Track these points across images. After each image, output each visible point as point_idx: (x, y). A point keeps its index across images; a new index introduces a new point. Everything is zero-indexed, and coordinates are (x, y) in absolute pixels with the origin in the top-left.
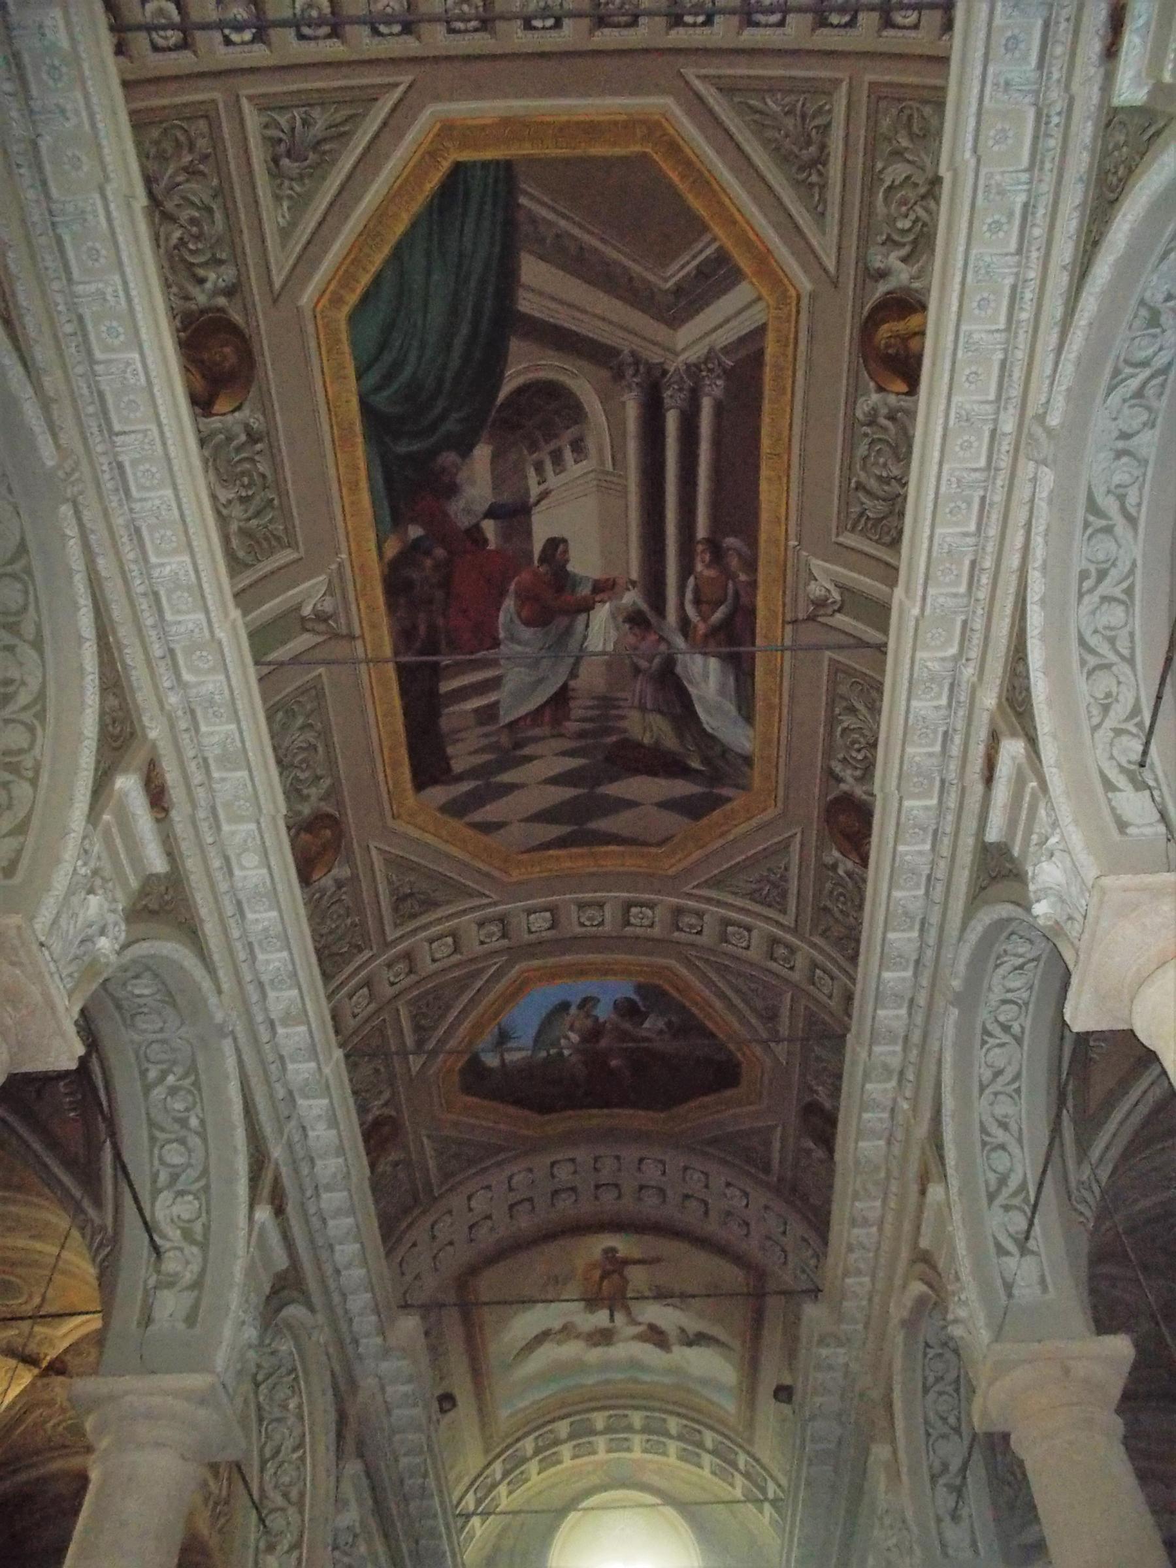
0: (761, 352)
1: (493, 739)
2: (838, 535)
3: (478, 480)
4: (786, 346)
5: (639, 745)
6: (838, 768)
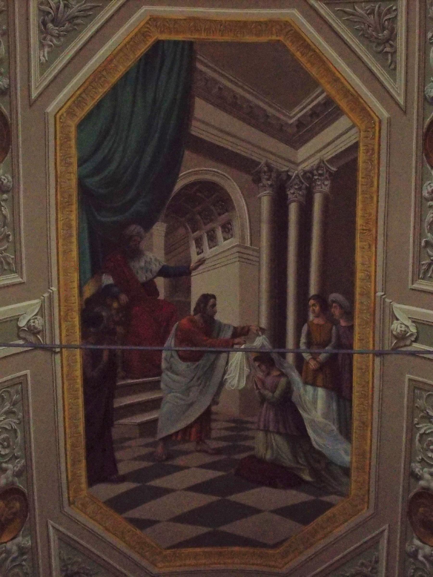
0: (355, 160)
1: (151, 449)
2: (413, 284)
3: (155, 248)
4: (373, 154)
5: (261, 461)
6: (417, 468)
